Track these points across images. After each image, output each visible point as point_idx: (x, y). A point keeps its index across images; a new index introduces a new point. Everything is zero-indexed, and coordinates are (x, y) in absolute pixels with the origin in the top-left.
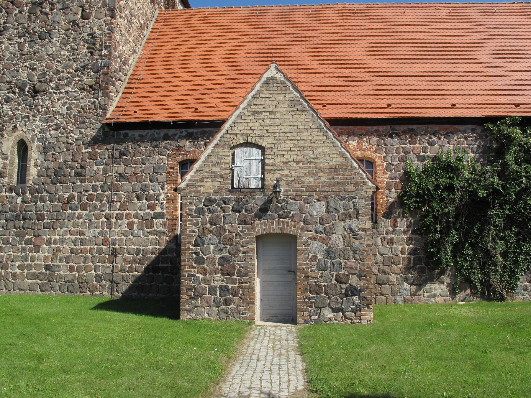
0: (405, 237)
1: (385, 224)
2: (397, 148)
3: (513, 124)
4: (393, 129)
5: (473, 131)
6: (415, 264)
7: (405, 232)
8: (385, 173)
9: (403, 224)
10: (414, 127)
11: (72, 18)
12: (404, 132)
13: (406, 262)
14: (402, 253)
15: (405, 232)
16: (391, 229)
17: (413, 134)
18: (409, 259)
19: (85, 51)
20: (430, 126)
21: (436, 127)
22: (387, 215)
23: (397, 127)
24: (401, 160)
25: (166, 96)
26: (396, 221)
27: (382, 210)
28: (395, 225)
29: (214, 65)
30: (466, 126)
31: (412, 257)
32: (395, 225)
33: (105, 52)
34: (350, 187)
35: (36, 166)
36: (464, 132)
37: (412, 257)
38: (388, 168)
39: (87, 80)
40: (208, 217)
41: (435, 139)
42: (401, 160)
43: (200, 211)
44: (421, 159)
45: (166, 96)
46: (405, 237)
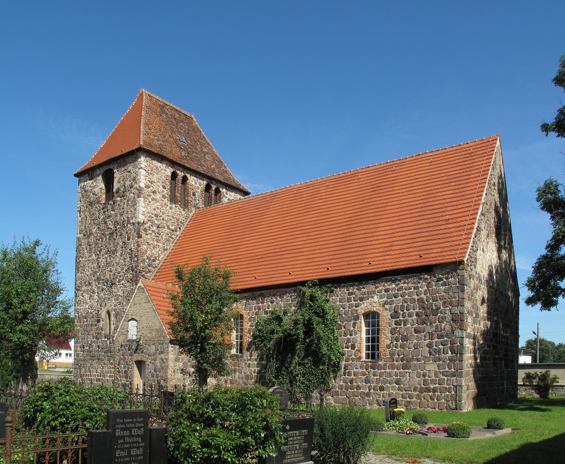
0: (256, 363)
1: (246, 354)
2: (255, 307)
3: (314, 285)
4: (253, 295)
5: (295, 291)
6: (260, 380)
7: (256, 360)
8: (248, 323)
9: (255, 355)
10: (263, 292)
11: (123, 240)
12: (259, 296)
13: (255, 378)
14: (254, 373)
15: (256, 360)
16: (249, 358)
17: (263, 296)
18: (257, 376)
19: (129, 259)
20: (272, 290)
21: (275, 291)
22: (248, 350)
23: (255, 293)
24: (257, 314)
25: (429, 198)
26: (252, 353)
27: (245, 346)
28: (251, 356)
29: (334, 202)
30: (291, 288)
31: (259, 375)
32: (251, 356)
33: (136, 259)
34: (162, 338)
35: (113, 324)
36: (290, 293)
37: (259, 375)
38: (250, 320)
39: (130, 276)
40: (121, 352)
41: (274, 299)
42: (257, 314)
43: (119, 350)
44: (266, 313)
45: (429, 198)
46: (256, 363)
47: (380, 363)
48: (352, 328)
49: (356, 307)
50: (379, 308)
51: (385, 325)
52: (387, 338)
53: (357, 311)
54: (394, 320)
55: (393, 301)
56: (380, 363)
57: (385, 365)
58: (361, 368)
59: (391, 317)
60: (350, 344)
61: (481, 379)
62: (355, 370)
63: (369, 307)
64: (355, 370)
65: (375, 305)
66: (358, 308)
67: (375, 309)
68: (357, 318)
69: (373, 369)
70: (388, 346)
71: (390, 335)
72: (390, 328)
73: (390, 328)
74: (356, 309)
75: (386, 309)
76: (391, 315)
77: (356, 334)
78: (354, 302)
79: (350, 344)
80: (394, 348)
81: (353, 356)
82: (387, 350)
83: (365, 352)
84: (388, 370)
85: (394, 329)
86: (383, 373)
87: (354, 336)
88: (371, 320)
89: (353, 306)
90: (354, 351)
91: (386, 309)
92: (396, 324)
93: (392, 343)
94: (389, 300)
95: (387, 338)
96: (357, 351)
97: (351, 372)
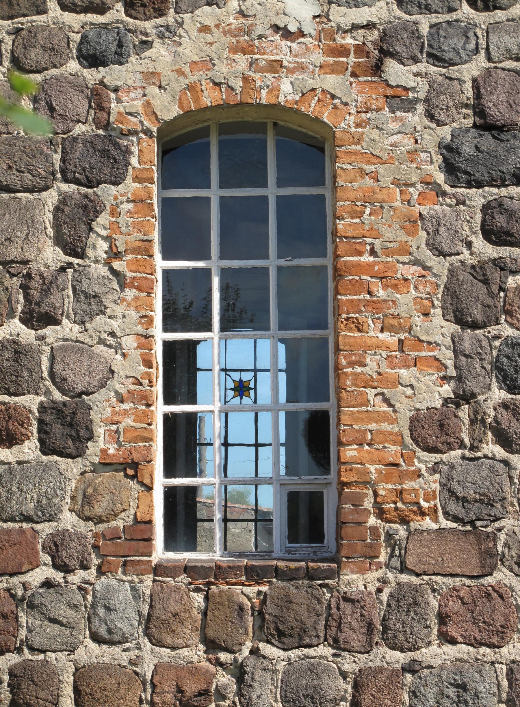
47: (355, 581)
48: (51, 256)
49: (92, 59)
50: (332, 82)
51: (393, 234)
52: (409, 349)
53: (97, 97)
54: (478, 198)
55: (467, 31)
56: (355, 581)
57: (406, 601)
58: (154, 627)
59: (450, 168)
60: (31, 402)
61: (44, 323)
62: (90, 652)
63: (232, 69)
64: (90, 652)
65: (284, 51)
66: (113, 74)
67: (287, 91)
68: (106, 158)
69: (282, 637)
70: (431, 431)
71: (440, 328)
72: (441, 266)
73: (441, 266)
74: (92, 76)
75: (399, 100)
76: (449, 151)
77: (91, 304)
78: (71, 19)
79: (31, 402)
80: (492, 448)
81: (68, 520)
82: (424, 460)
83: (274, 527)
84: (435, 654)
85: (480, 272)
86: (395, 675)
87: (69, 328)
88: (215, 194)
89: (55, 54)
90: (72, 468)
91: (399, 100)
92: (492, 235)
93: (463, 397)
94: (424, 23)
95: (409, 349)
96: (106, 464)
97: (49, 676)
